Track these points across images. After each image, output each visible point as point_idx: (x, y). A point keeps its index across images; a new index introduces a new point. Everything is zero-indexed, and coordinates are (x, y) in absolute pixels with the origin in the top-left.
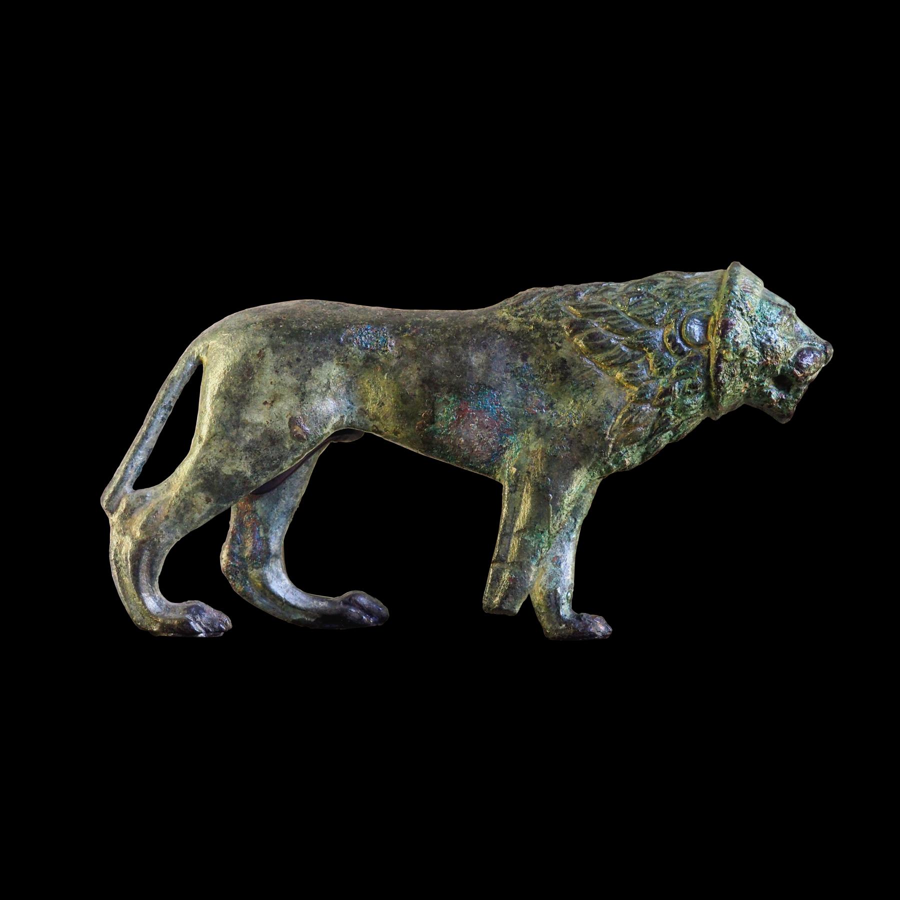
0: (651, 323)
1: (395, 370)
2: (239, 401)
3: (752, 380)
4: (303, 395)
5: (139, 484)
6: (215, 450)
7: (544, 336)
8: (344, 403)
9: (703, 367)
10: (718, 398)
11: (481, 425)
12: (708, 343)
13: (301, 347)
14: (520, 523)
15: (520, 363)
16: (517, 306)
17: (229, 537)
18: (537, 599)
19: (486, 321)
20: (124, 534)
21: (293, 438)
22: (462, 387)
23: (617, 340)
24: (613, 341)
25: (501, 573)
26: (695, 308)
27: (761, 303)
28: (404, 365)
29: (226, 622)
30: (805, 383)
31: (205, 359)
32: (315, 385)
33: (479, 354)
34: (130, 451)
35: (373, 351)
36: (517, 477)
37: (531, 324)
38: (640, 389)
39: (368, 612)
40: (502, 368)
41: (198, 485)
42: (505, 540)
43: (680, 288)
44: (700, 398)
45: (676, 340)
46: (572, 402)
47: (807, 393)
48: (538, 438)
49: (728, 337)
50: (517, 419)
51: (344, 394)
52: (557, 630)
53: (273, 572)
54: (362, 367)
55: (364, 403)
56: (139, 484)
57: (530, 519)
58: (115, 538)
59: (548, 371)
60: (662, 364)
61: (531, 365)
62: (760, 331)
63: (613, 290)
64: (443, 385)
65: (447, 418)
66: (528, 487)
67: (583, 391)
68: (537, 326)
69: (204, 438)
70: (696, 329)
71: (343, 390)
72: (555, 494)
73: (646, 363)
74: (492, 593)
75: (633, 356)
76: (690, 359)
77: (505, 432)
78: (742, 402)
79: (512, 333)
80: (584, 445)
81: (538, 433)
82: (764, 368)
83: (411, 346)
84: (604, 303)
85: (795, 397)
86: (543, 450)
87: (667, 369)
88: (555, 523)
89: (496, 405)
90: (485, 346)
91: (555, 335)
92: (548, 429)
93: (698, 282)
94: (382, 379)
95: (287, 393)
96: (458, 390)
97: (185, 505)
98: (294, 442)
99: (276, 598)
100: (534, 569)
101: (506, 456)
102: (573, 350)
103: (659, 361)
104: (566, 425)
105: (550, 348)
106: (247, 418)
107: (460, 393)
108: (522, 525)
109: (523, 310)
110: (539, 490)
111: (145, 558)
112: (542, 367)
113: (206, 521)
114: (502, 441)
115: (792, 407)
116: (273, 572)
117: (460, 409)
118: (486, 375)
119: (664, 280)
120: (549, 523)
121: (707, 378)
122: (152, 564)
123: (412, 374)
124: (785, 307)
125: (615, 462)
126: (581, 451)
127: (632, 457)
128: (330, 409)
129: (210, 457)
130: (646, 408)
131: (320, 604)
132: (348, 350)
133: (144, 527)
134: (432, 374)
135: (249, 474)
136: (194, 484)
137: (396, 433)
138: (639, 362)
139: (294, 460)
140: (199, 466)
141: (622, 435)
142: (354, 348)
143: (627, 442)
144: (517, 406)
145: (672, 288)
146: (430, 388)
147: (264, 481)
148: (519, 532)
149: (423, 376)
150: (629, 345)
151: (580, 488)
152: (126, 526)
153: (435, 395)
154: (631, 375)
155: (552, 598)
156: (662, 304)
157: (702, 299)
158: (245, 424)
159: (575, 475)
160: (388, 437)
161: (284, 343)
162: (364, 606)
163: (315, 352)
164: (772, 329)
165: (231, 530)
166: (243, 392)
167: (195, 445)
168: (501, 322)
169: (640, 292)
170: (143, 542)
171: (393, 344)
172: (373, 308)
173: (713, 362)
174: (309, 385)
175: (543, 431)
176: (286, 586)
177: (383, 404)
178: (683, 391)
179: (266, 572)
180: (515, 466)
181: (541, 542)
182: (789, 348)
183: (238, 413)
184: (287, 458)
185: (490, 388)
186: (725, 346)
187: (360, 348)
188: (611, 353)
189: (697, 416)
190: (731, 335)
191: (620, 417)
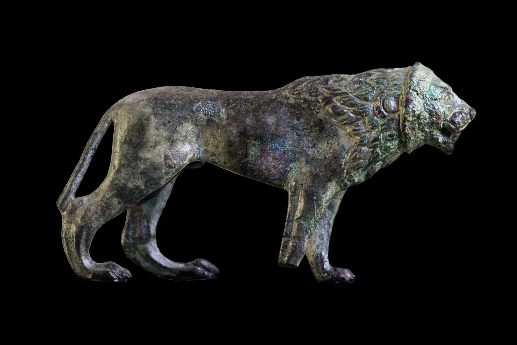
0: (367, 100)
1: (225, 127)
2: (137, 145)
3: (426, 132)
4: (172, 142)
5: (80, 193)
6: (124, 173)
7: (309, 106)
8: (195, 146)
9: (396, 124)
10: (406, 142)
11: (274, 158)
12: (399, 111)
13: (173, 115)
14: (298, 214)
15: (296, 122)
16: (294, 88)
17: (126, 225)
18: (311, 259)
19: (276, 97)
20: (71, 223)
21: (166, 166)
22: (263, 137)
23: (347, 110)
24: (345, 110)
25: (288, 243)
26: (391, 90)
27: (430, 87)
28: (229, 125)
29: (128, 273)
30: (458, 132)
31: (115, 121)
32: (179, 136)
33: (272, 118)
34: (73, 175)
35: (211, 116)
36: (295, 187)
37: (302, 99)
38: (361, 138)
39: (208, 270)
40: (285, 125)
41: (114, 194)
42: (290, 224)
43: (384, 78)
44: (396, 142)
45: (380, 109)
46: (326, 144)
47: (460, 137)
48: (307, 164)
49: (409, 107)
50: (295, 154)
51: (195, 141)
52: (323, 277)
53: (152, 246)
54: (206, 125)
55: (207, 146)
56: (80, 193)
57: (304, 211)
58: (64, 226)
59: (312, 126)
60: (373, 123)
61: (302, 123)
62: (428, 103)
63: (346, 80)
64: (252, 135)
65: (255, 155)
66: (302, 192)
67: (332, 137)
68: (305, 100)
69: (117, 166)
70: (392, 104)
71: (195, 139)
72: (318, 197)
73: (364, 122)
74: (283, 255)
75: (356, 119)
76: (389, 120)
77: (288, 161)
78: (423, 143)
79: (291, 104)
80: (332, 170)
81: (307, 161)
82: (432, 124)
83: (233, 113)
84: (340, 88)
85: (453, 140)
86: (310, 172)
87: (375, 126)
88: (318, 213)
89: (283, 146)
90: (275, 112)
91: (316, 105)
92: (313, 159)
93: (394, 74)
94: (217, 132)
95: (163, 141)
96: (260, 138)
97: (106, 206)
98: (167, 169)
99: (154, 262)
100: (307, 240)
101: (289, 175)
102: (326, 114)
103: (371, 120)
104: (323, 157)
105: (312, 113)
106: (142, 155)
107: (261, 140)
108: (299, 215)
109: (297, 90)
110: (308, 194)
111: (84, 236)
112: (308, 124)
113: (118, 214)
114: (287, 167)
115: (451, 146)
116: (152, 246)
117: (262, 149)
118: (276, 129)
119: (375, 73)
120: (314, 214)
121: (399, 131)
122: (87, 239)
123: (234, 130)
124: (445, 88)
125: (349, 181)
126: (332, 172)
127: (359, 177)
128: (188, 149)
129: (121, 178)
130: (365, 149)
131: (180, 266)
132: (197, 116)
133: (83, 218)
134: (245, 129)
135: (143, 187)
136: (112, 194)
137: (225, 163)
138: (360, 122)
139: (167, 179)
140: (114, 183)
141: (351, 165)
142: (201, 115)
143: (354, 169)
144: (295, 147)
145: (379, 78)
146: (244, 137)
147: (151, 191)
148: (297, 219)
149: (240, 131)
150: (354, 112)
151: (332, 193)
152: (72, 218)
153: (247, 141)
154: (355, 130)
155: (319, 258)
156: (373, 88)
157: (395, 85)
158: (140, 159)
159: (329, 185)
160: (221, 166)
161: (161, 112)
162: (205, 267)
163: (179, 117)
164: (436, 101)
165: (127, 221)
166: (139, 141)
167: (111, 172)
168: (285, 98)
169: (361, 81)
170: (83, 227)
171: (224, 112)
172: (211, 90)
173: (401, 121)
174: (176, 136)
175: (310, 161)
176: (159, 255)
177: (218, 147)
178: (386, 139)
179: (148, 246)
180: (294, 181)
181: (310, 224)
182: (448, 113)
183: (137, 153)
184: (163, 178)
185: (279, 137)
186: (407, 113)
187: (205, 114)
188: (344, 117)
189: (395, 152)
190: (411, 106)
191: (350, 154)
